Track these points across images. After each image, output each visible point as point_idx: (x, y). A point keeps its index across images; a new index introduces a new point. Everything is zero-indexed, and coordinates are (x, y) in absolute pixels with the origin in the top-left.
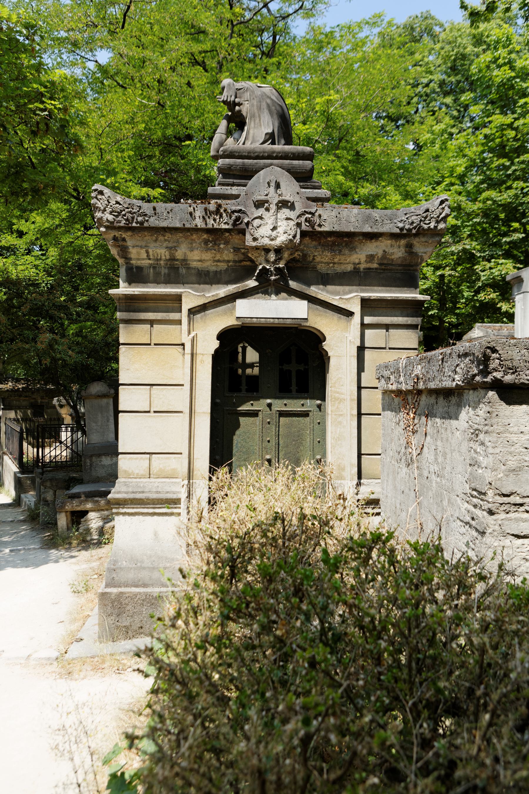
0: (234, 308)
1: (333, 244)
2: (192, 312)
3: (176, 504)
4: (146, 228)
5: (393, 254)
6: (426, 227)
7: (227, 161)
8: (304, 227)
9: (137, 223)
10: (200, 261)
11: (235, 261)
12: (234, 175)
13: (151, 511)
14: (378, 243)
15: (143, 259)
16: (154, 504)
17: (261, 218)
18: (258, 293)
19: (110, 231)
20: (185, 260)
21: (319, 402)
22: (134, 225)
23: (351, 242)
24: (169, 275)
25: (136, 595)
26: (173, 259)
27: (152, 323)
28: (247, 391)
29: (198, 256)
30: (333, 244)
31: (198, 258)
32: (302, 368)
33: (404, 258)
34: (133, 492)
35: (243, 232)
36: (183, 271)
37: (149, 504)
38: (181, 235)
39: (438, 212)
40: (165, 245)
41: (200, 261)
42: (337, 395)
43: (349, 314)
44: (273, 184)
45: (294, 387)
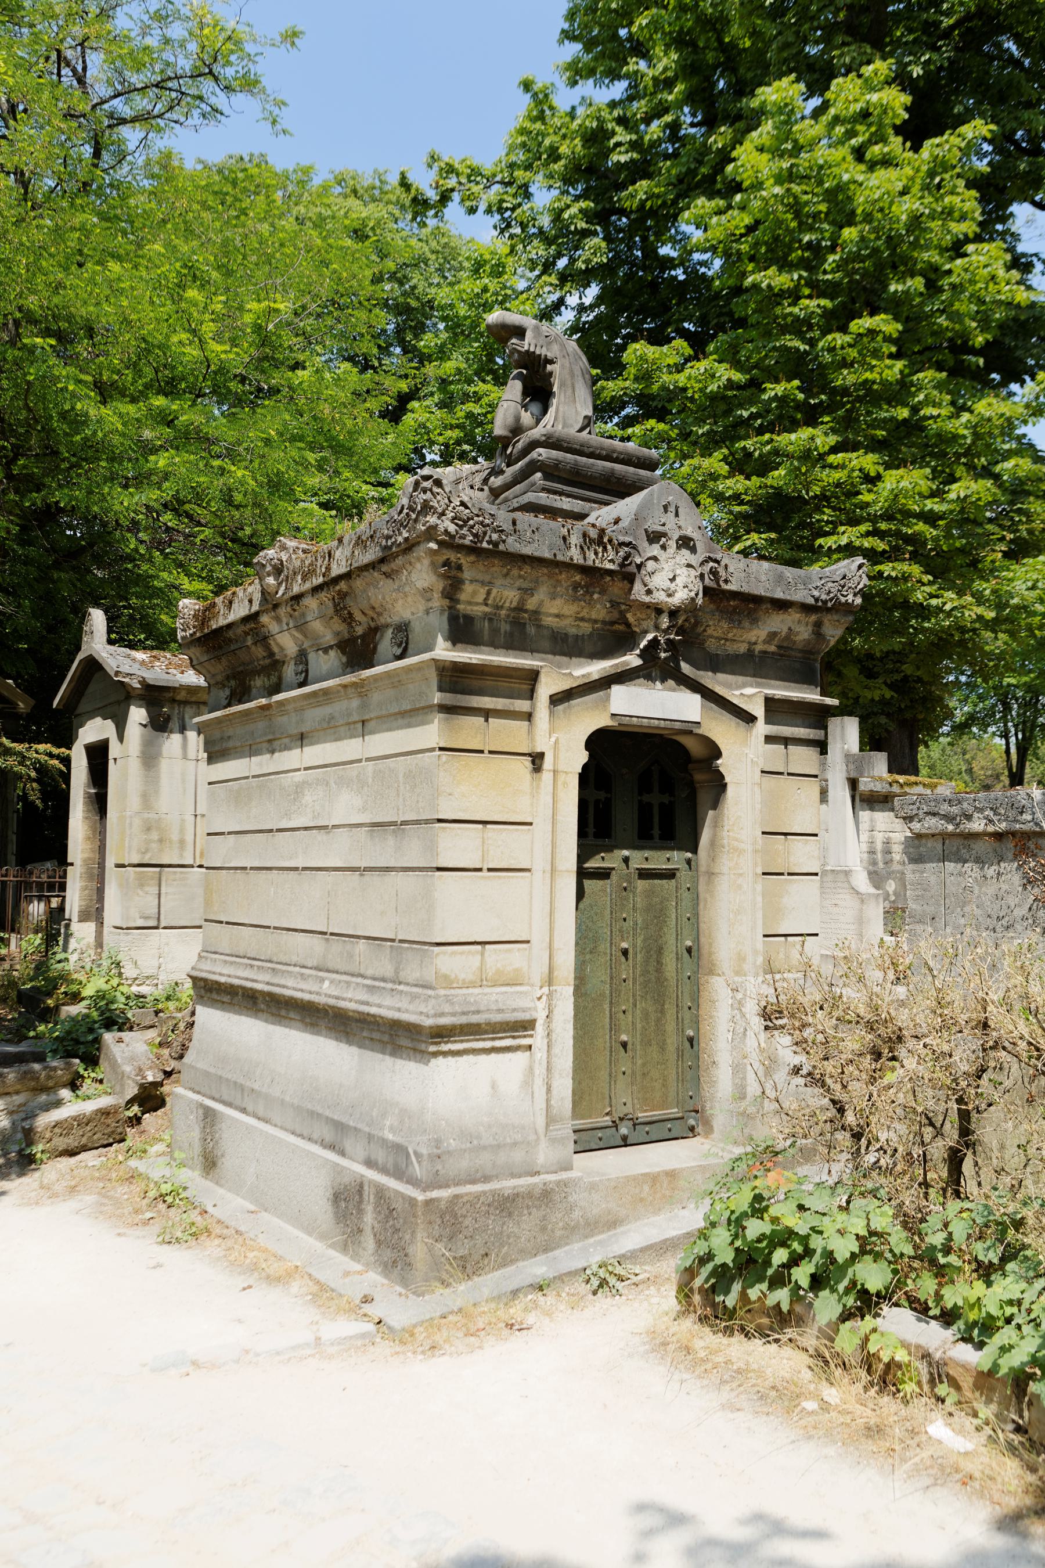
0: (608, 698)
1: (734, 611)
2: (556, 700)
3: (525, 1029)
4: (502, 552)
5: (798, 633)
6: (843, 599)
7: (554, 454)
8: (707, 581)
9: (489, 542)
10: (557, 616)
11: (604, 622)
12: (559, 477)
13: (488, 1044)
14: (786, 616)
15: (477, 604)
16: (493, 1032)
17: (655, 559)
18: (638, 677)
19: (445, 551)
20: (536, 612)
21: (689, 855)
22: (485, 545)
23: (755, 610)
24: (511, 634)
25: (478, 1196)
26: (520, 609)
27: (487, 714)
28: (596, 836)
29: (557, 608)
30: (734, 611)
31: (556, 611)
32: (666, 799)
33: (808, 642)
34: (464, 1013)
35: (630, 579)
36: (531, 630)
37: (486, 1032)
38: (545, 571)
39: (856, 579)
40: (518, 584)
41: (557, 616)
42: (736, 843)
43: (749, 719)
44: (672, 509)
45: (656, 832)
